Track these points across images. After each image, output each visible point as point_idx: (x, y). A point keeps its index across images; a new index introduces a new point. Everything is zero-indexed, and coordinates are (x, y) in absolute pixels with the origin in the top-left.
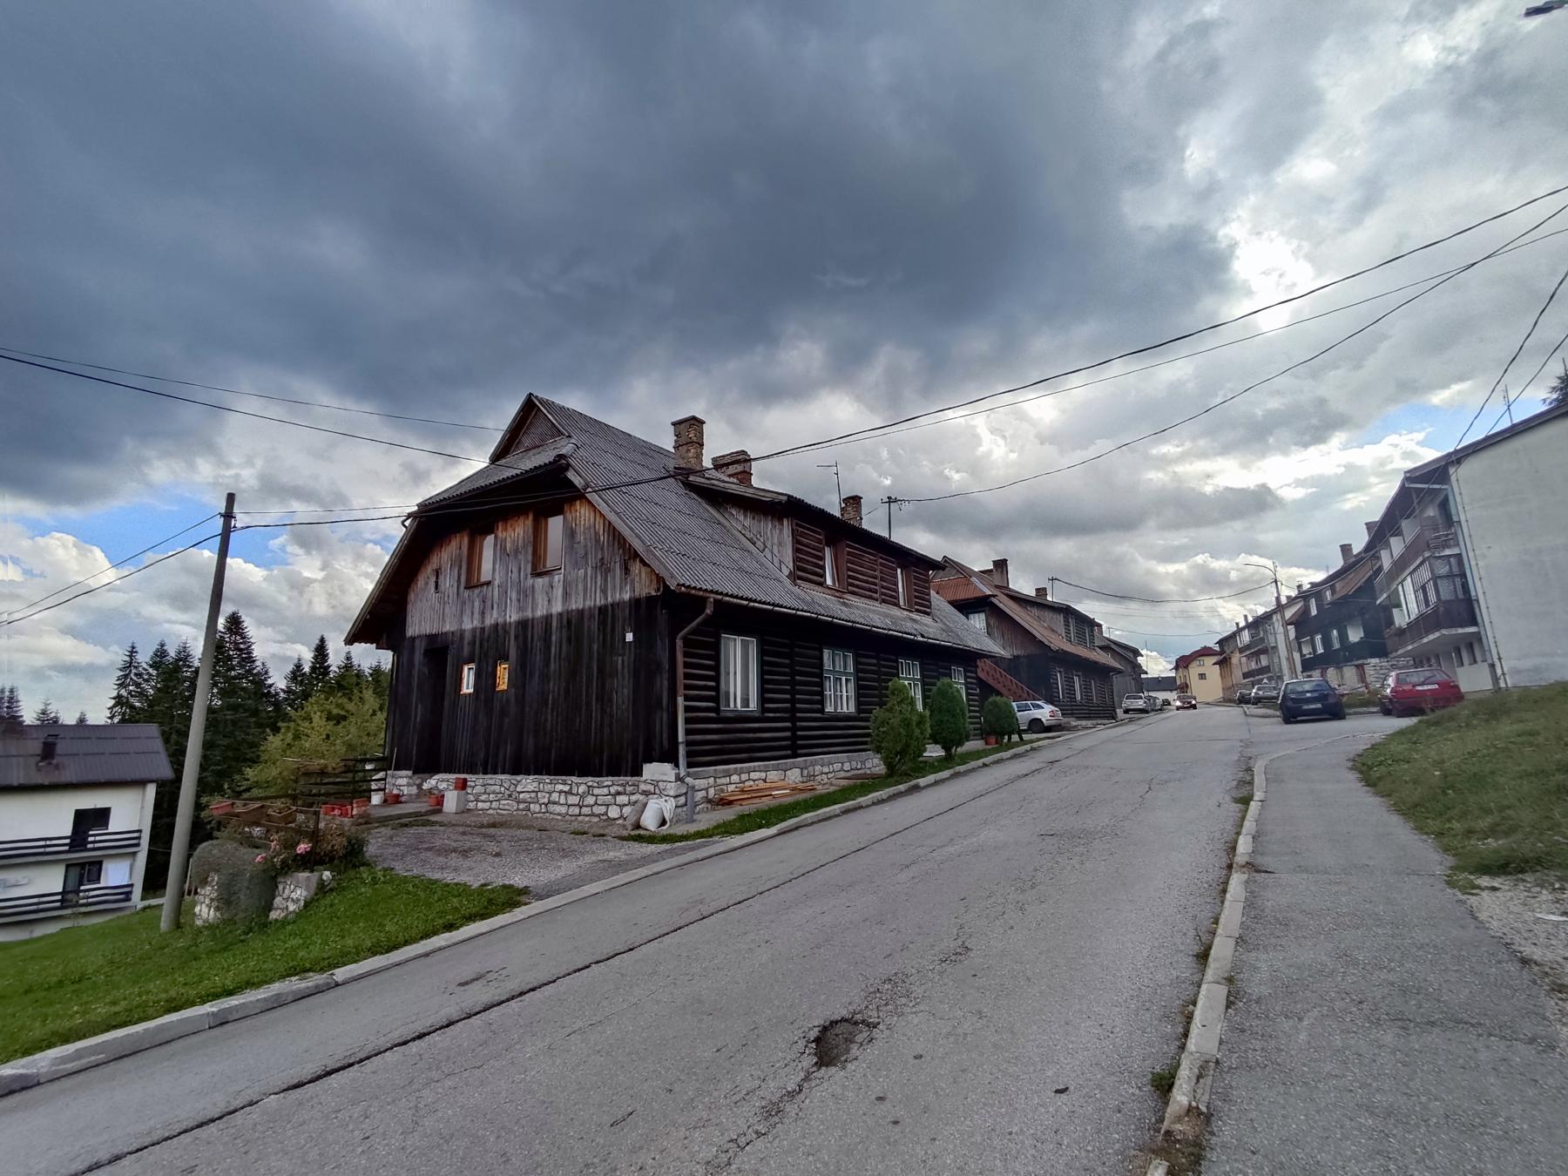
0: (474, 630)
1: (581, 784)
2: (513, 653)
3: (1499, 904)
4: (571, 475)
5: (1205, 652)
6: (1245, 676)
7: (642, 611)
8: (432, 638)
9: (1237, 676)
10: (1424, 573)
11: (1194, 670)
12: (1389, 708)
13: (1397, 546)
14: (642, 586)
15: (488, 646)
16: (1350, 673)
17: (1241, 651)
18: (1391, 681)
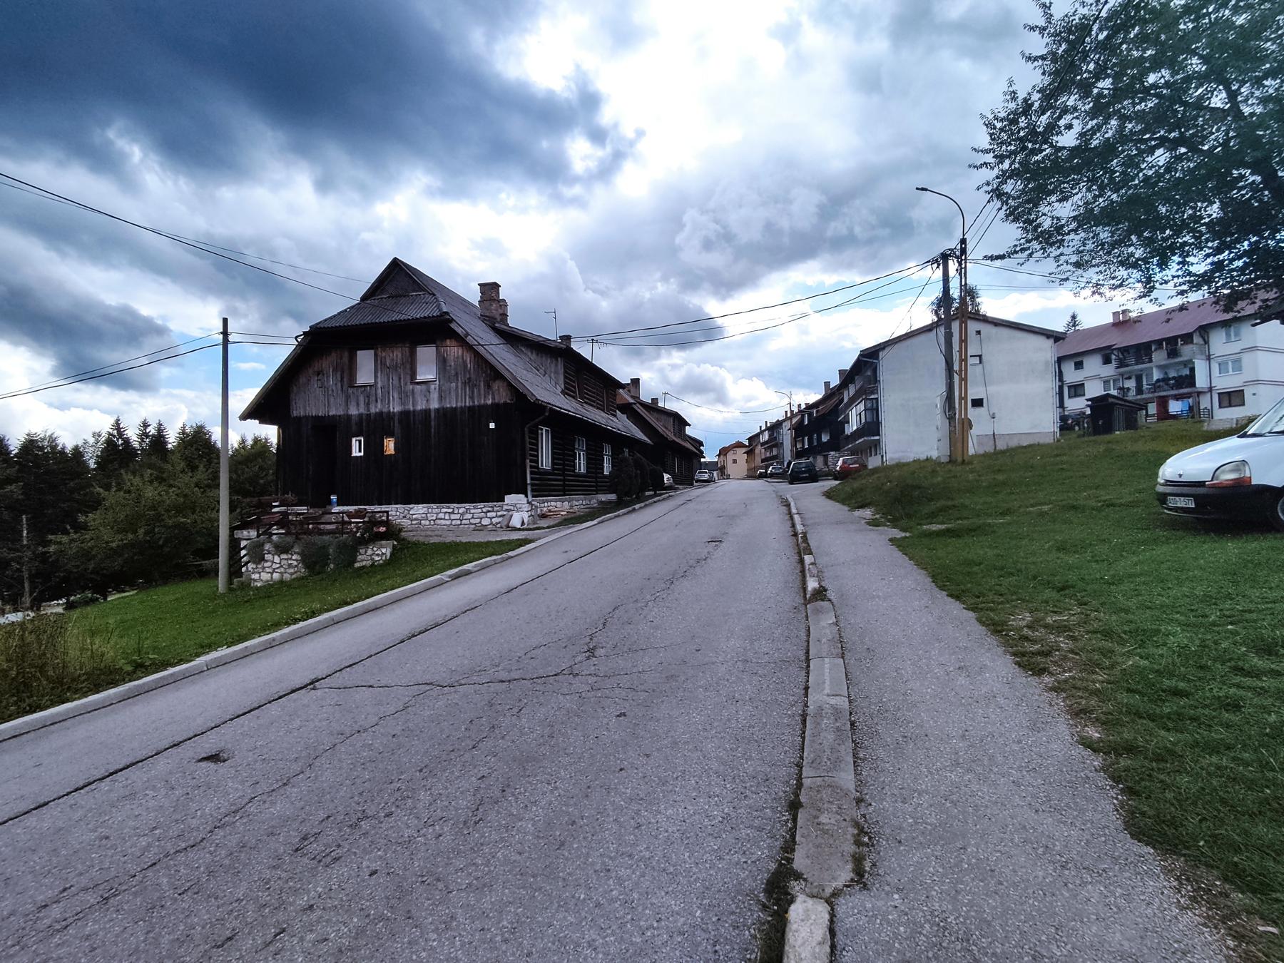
0: (360, 415)
1: (462, 508)
3: (857, 513)
4: (453, 326)
5: (739, 445)
7: (496, 411)
8: (317, 418)
9: (758, 460)
10: (861, 407)
11: (730, 456)
12: (836, 476)
13: (852, 390)
15: (375, 427)
16: (820, 460)
17: (762, 445)
18: (840, 463)
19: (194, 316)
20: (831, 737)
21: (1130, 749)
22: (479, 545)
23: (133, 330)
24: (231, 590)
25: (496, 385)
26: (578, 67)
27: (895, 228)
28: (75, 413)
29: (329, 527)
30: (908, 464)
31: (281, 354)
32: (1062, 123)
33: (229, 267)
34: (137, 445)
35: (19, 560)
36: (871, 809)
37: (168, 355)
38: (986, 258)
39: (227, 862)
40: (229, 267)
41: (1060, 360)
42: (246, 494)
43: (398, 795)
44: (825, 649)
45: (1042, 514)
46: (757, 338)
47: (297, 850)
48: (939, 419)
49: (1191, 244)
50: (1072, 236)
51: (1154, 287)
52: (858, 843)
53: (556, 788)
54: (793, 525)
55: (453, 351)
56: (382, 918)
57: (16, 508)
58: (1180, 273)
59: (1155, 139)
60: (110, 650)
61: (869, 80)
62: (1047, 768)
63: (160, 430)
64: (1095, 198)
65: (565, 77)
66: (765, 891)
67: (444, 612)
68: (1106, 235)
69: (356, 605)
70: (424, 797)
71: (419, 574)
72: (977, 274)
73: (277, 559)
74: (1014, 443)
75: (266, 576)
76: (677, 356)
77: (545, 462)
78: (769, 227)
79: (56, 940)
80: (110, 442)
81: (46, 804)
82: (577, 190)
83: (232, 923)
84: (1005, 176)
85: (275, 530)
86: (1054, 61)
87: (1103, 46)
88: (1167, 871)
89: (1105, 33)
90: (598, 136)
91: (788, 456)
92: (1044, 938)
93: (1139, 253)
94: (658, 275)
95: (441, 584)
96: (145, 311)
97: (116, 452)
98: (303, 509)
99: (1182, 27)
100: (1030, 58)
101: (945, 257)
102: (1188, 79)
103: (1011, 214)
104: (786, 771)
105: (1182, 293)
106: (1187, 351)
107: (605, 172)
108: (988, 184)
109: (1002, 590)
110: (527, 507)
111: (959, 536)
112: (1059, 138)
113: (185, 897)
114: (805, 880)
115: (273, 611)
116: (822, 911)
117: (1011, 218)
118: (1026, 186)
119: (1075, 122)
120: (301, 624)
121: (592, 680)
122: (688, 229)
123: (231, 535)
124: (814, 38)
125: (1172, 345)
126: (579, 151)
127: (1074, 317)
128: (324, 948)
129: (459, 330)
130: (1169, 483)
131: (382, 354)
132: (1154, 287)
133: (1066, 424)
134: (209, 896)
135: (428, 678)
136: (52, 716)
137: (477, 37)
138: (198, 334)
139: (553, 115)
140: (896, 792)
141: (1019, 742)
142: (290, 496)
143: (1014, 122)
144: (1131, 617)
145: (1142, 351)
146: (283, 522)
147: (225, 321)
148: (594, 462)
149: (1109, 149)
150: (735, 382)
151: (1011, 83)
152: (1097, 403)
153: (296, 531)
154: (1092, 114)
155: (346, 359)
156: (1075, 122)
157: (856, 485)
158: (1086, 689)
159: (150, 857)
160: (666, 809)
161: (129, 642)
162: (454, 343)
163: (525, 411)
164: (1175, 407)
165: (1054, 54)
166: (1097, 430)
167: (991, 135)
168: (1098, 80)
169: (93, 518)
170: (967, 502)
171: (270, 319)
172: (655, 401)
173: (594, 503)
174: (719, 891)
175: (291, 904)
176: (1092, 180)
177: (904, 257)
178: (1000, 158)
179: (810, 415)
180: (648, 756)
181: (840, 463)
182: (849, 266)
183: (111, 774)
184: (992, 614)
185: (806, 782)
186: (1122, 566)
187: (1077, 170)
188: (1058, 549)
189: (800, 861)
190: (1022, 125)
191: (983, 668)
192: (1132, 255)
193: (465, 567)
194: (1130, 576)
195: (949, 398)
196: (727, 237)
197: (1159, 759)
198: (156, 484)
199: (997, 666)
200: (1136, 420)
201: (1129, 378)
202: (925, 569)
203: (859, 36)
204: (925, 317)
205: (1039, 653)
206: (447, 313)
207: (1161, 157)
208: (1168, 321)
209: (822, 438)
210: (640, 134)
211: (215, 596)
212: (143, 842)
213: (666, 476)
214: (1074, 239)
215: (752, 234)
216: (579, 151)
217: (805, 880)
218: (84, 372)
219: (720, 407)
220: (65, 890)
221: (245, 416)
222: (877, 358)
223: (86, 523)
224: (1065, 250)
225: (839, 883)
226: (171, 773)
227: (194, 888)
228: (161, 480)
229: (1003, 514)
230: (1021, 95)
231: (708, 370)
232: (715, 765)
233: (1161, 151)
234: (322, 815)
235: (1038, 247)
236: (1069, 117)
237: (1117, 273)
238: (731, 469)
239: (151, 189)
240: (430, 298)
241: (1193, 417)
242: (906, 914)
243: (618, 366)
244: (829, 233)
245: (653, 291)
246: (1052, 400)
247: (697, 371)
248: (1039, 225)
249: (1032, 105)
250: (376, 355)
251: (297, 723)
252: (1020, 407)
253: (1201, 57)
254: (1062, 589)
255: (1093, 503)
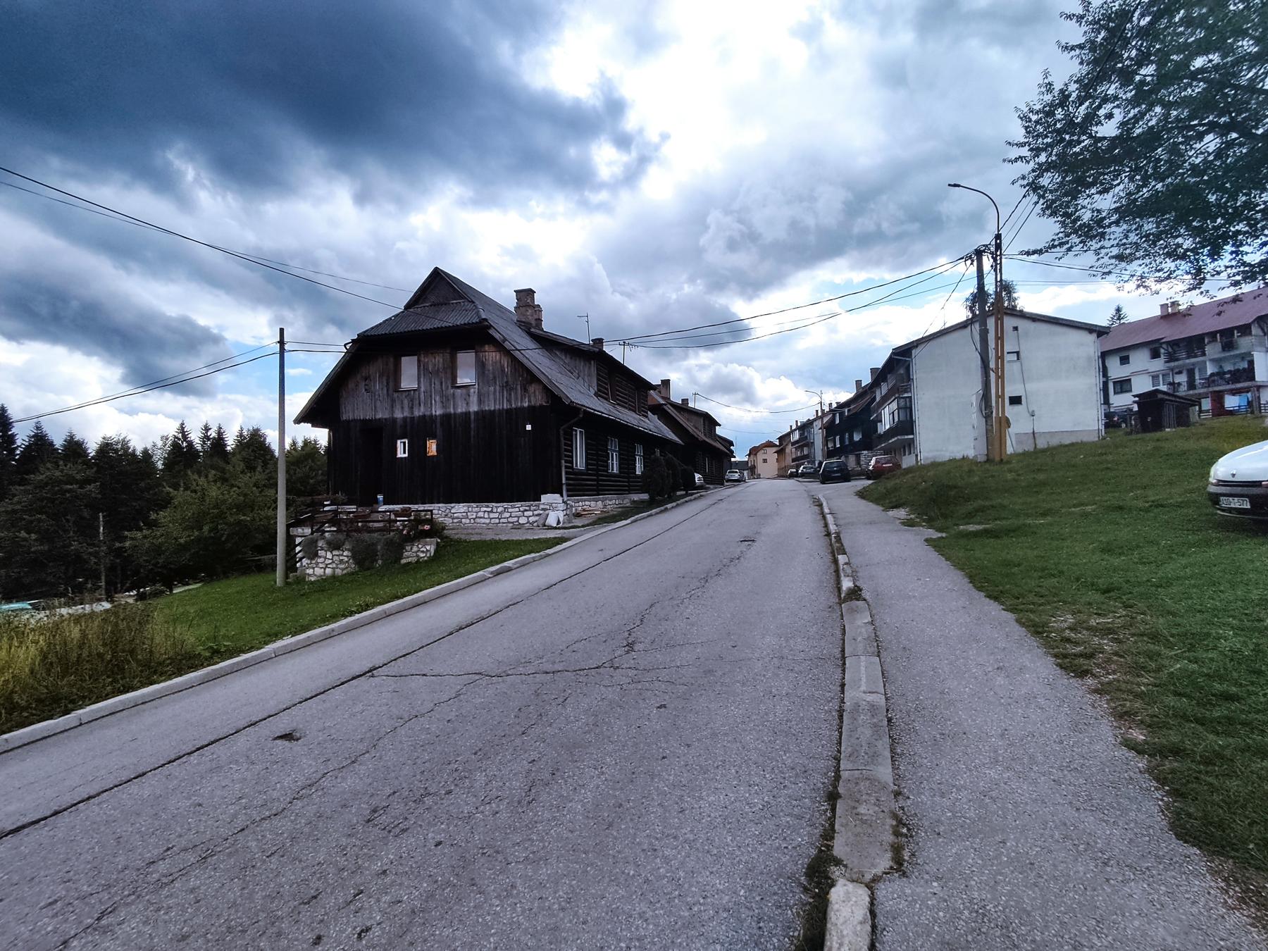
0: (405, 419)
1: (500, 507)
2: (439, 432)
3: (891, 513)
4: (491, 331)
5: (769, 444)
6: (794, 460)
7: (532, 413)
8: (364, 422)
9: (789, 461)
10: (894, 406)
11: (761, 456)
12: (869, 475)
13: (884, 388)
14: (536, 398)
15: (418, 430)
16: (852, 459)
17: (793, 444)
18: (873, 462)
19: (251, 326)
20: (868, 732)
21: (1177, 751)
22: (518, 543)
23: (193, 339)
24: (287, 584)
25: (532, 389)
26: (602, 74)
27: (924, 224)
28: (142, 418)
29: (376, 525)
30: (943, 464)
31: (329, 362)
32: (1102, 112)
33: (283, 280)
34: (199, 448)
35: (96, 554)
36: (909, 802)
37: (224, 363)
38: (1021, 253)
39: (306, 830)
40: (283, 280)
41: (1104, 355)
42: (300, 493)
43: (455, 775)
44: (861, 647)
45: (1085, 515)
46: (785, 337)
47: (369, 821)
48: (975, 418)
49: (1245, 233)
50: (1113, 228)
51: (1204, 279)
52: (897, 834)
53: (603, 773)
54: (826, 525)
55: (492, 356)
56: (448, 883)
57: (95, 507)
58: (1234, 263)
59: (1204, 125)
60: (190, 638)
61: (893, 74)
62: (1089, 767)
63: (220, 433)
64: (1139, 188)
65: (590, 85)
66: (806, 874)
67: (487, 607)
68: (1150, 226)
69: (406, 599)
70: (480, 778)
71: (461, 570)
72: (1010, 271)
73: (329, 555)
74: (1055, 442)
75: (319, 571)
76: (704, 357)
77: (580, 462)
78: (794, 225)
79: (165, 892)
80: (176, 445)
81: (144, 774)
82: (603, 196)
83: (315, 884)
84: (1042, 169)
85: (327, 528)
86: (1093, 50)
87: (1143, 33)
88: (1214, 873)
89: (1148, 19)
90: (623, 142)
91: (819, 456)
92: (1084, 929)
93: (1188, 243)
94: (684, 277)
95: (484, 580)
96: (202, 321)
97: (181, 453)
98: (352, 508)
99: (1232, 8)
100: (1067, 48)
101: (979, 253)
102: (1238, 62)
103: (1047, 208)
104: (825, 764)
105: (1236, 284)
106: (1244, 343)
107: (631, 177)
108: (1024, 178)
109: (1043, 591)
110: (562, 506)
111: (997, 537)
112: (1099, 128)
113: (273, 859)
114: (845, 866)
115: (328, 605)
116: (862, 895)
117: (1048, 212)
118: (1064, 178)
119: (1116, 111)
120: (357, 616)
121: (631, 673)
122: (711, 231)
123: (288, 531)
124: (837, 34)
125: (1227, 337)
126: (605, 158)
127: (1118, 310)
128: (399, 909)
129: (497, 336)
130: (1221, 483)
131: (424, 359)
132: (1204, 279)
133: (1112, 422)
134: (294, 859)
135: (476, 668)
136: (143, 696)
137: (504, 50)
138: (251, 342)
139: (580, 123)
140: (934, 786)
141: (1061, 742)
142: (340, 496)
143: (1050, 114)
144: (1178, 620)
145: (1195, 344)
146: (334, 521)
147: (282, 331)
148: (627, 463)
149: (1153, 137)
150: (763, 380)
151: (1046, 74)
152: (1144, 399)
153: (347, 530)
154: (1134, 102)
155: (391, 366)
156: (1116, 111)
157: (890, 484)
158: (1130, 692)
159: (241, 821)
160: (708, 795)
161: (205, 630)
162: (492, 349)
163: (560, 413)
164: (1231, 402)
165: (1092, 42)
166: (1146, 428)
167: (1026, 128)
168: (1140, 66)
169: (163, 516)
170: (1006, 502)
171: (315, 326)
172: (685, 401)
173: (627, 503)
174: (762, 873)
175: (367, 869)
176: (1137, 170)
177: (935, 252)
178: (1037, 151)
179: (841, 414)
180: (689, 746)
181: (873, 462)
182: (878, 263)
183: (198, 749)
184: (1032, 616)
185: (845, 775)
186: (1170, 569)
187: (1118, 160)
188: (1103, 551)
189: (839, 848)
190: (1059, 117)
191: (1022, 669)
192: (1179, 246)
193: (506, 564)
194: (1178, 578)
195: (986, 397)
196: (752, 237)
197: (1208, 762)
198: (219, 484)
199: (1037, 667)
200: (1188, 416)
201: (1180, 372)
202: (962, 569)
203: (885, 28)
204: (960, 313)
205: (1081, 655)
206: (485, 320)
207: (1211, 142)
208: (1219, 314)
209: (857, 437)
210: (665, 137)
211: (273, 589)
212: (232, 809)
213: (697, 476)
214: (1117, 232)
215: (776, 233)
216: (605, 158)
217: (845, 866)
218: (150, 379)
219: (748, 406)
220: (168, 849)
221: (299, 420)
222: (910, 356)
223: (155, 520)
224: (1107, 244)
225: (878, 871)
226: (250, 749)
227: (280, 851)
228: (224, 480)
229: (1044, 515)
230: (1058, 86)
231: (736, 369)
232: (754, 756)
233: (1211, 136)
234: (388, 791)
235: (1078, 240)
236: (1109, 106)
237: (1163, 265)
238: (761, 468)
239: (209, 210)
240: (470, 306)
241: (1252, 412)
242: (946, 901)
243: (651, 371)
244: (856, 230)
245: (679, 292)
246: (1096, 397)
247: (725, 370)
248: (1079, 218)
249: (1069, 95)
250: (419, 361)
251: (359, 707)
252: (1062, 404)
253: (1252, 38)
254: (1107, 591)
255: (1140, 504)
